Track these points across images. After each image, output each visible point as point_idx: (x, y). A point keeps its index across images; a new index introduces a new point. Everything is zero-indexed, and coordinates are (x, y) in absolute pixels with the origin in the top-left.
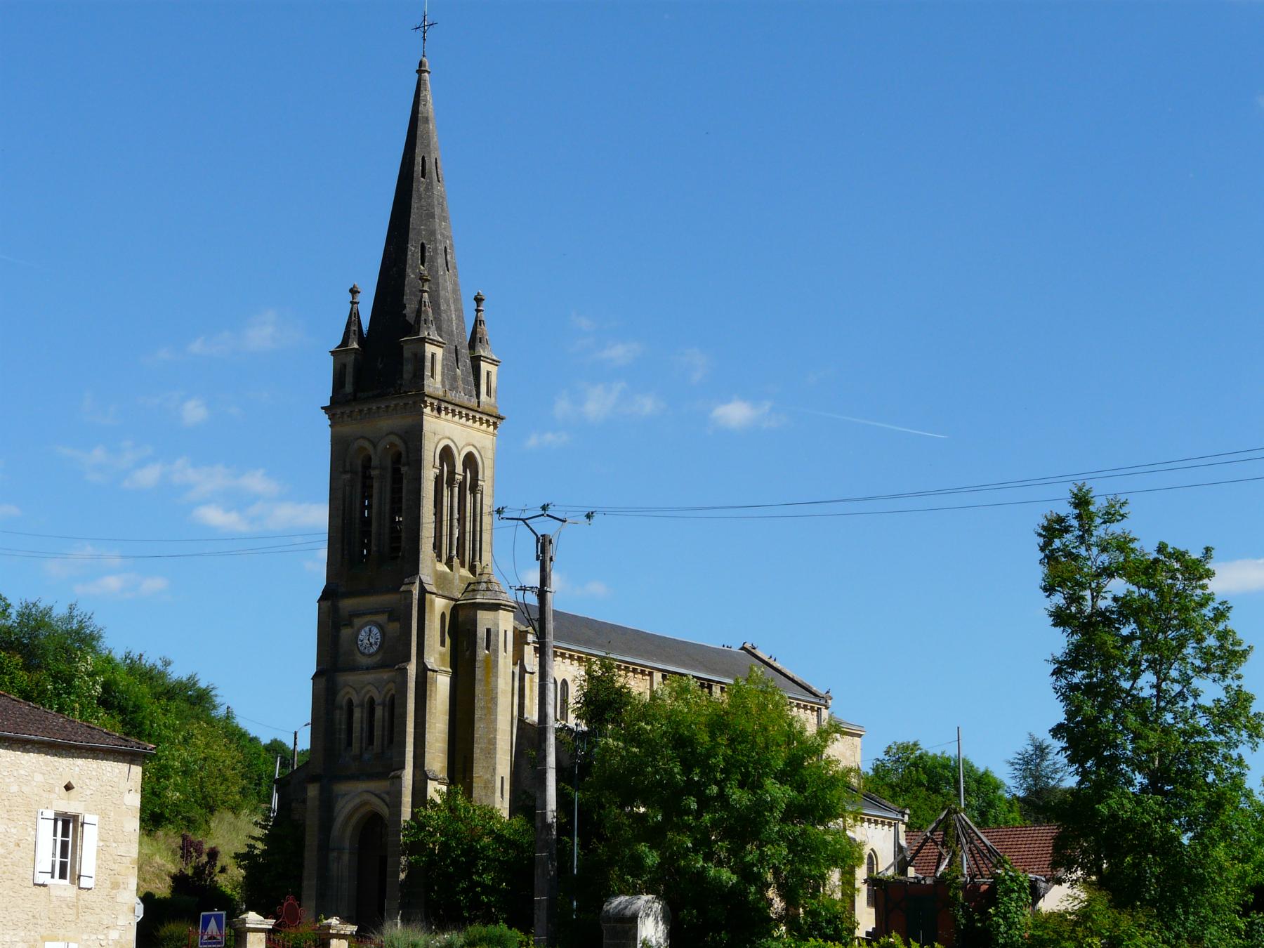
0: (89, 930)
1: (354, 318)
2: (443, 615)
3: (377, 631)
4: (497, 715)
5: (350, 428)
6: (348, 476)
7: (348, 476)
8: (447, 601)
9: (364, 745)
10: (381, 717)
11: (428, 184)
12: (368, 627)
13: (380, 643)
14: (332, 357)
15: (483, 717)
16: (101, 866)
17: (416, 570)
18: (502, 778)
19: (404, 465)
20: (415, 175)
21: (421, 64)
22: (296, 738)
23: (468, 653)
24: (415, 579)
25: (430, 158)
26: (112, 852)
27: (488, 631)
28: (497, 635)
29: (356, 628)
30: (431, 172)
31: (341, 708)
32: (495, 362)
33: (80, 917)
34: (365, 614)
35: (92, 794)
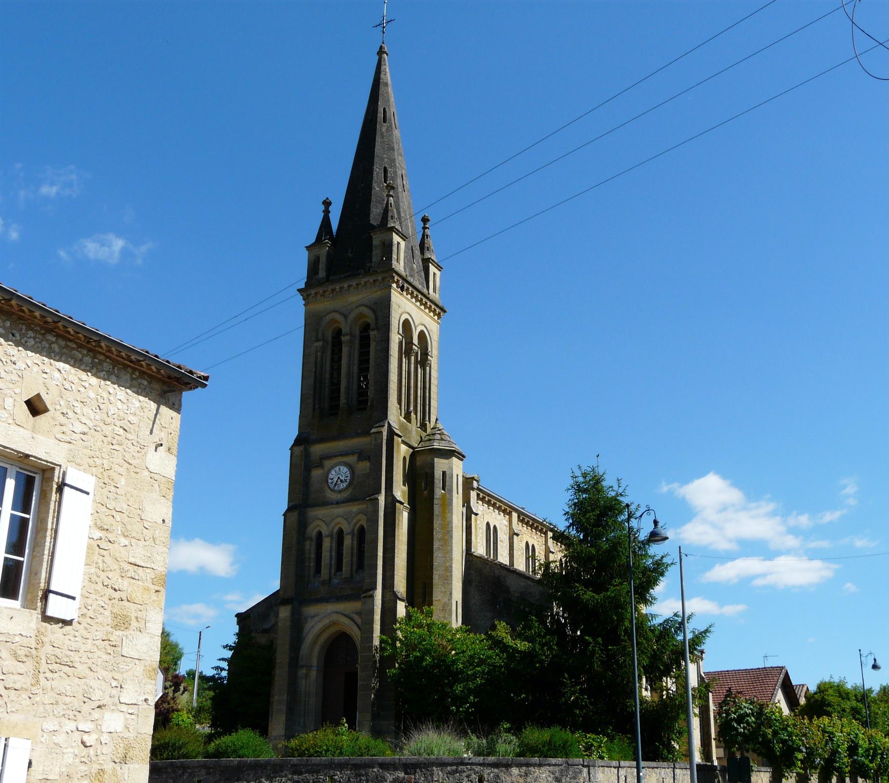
0: (59, 710)
1: (326, 222)
2: (405, 458)
3: (347, 470)
4: (452, 546)
5: (322, 305)
6: (320, 344)
7: (320, 344)
8: (408, 448)
9: (333, 571)
10: (351, 545)
11: (388, 127)
12: (338, 467)
13: (350, 480)
14: (307, 252)
15: (441, 547)
16: (94, 578)
17: (385, 415)
18: (457, 602)
19: (373, 330)
20: (378, 120)
21: (381, 47)
22: (200, 635)
23: (426, 492)
24: (384, 423)
25: (390, 110)
26: (118, 555)
27: (444, 473)
28: (452, 478)
29: (326, 469)
30: (390, 119)
31: (311, 539)
32: (439, 268)
33: (43, 681)
34: (336, 456)
35: (84, 434)
